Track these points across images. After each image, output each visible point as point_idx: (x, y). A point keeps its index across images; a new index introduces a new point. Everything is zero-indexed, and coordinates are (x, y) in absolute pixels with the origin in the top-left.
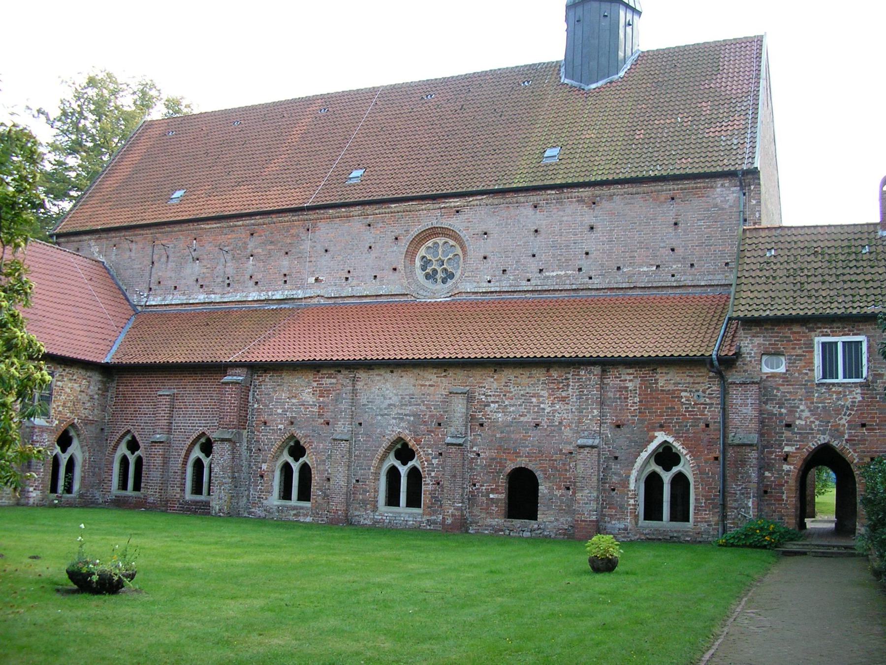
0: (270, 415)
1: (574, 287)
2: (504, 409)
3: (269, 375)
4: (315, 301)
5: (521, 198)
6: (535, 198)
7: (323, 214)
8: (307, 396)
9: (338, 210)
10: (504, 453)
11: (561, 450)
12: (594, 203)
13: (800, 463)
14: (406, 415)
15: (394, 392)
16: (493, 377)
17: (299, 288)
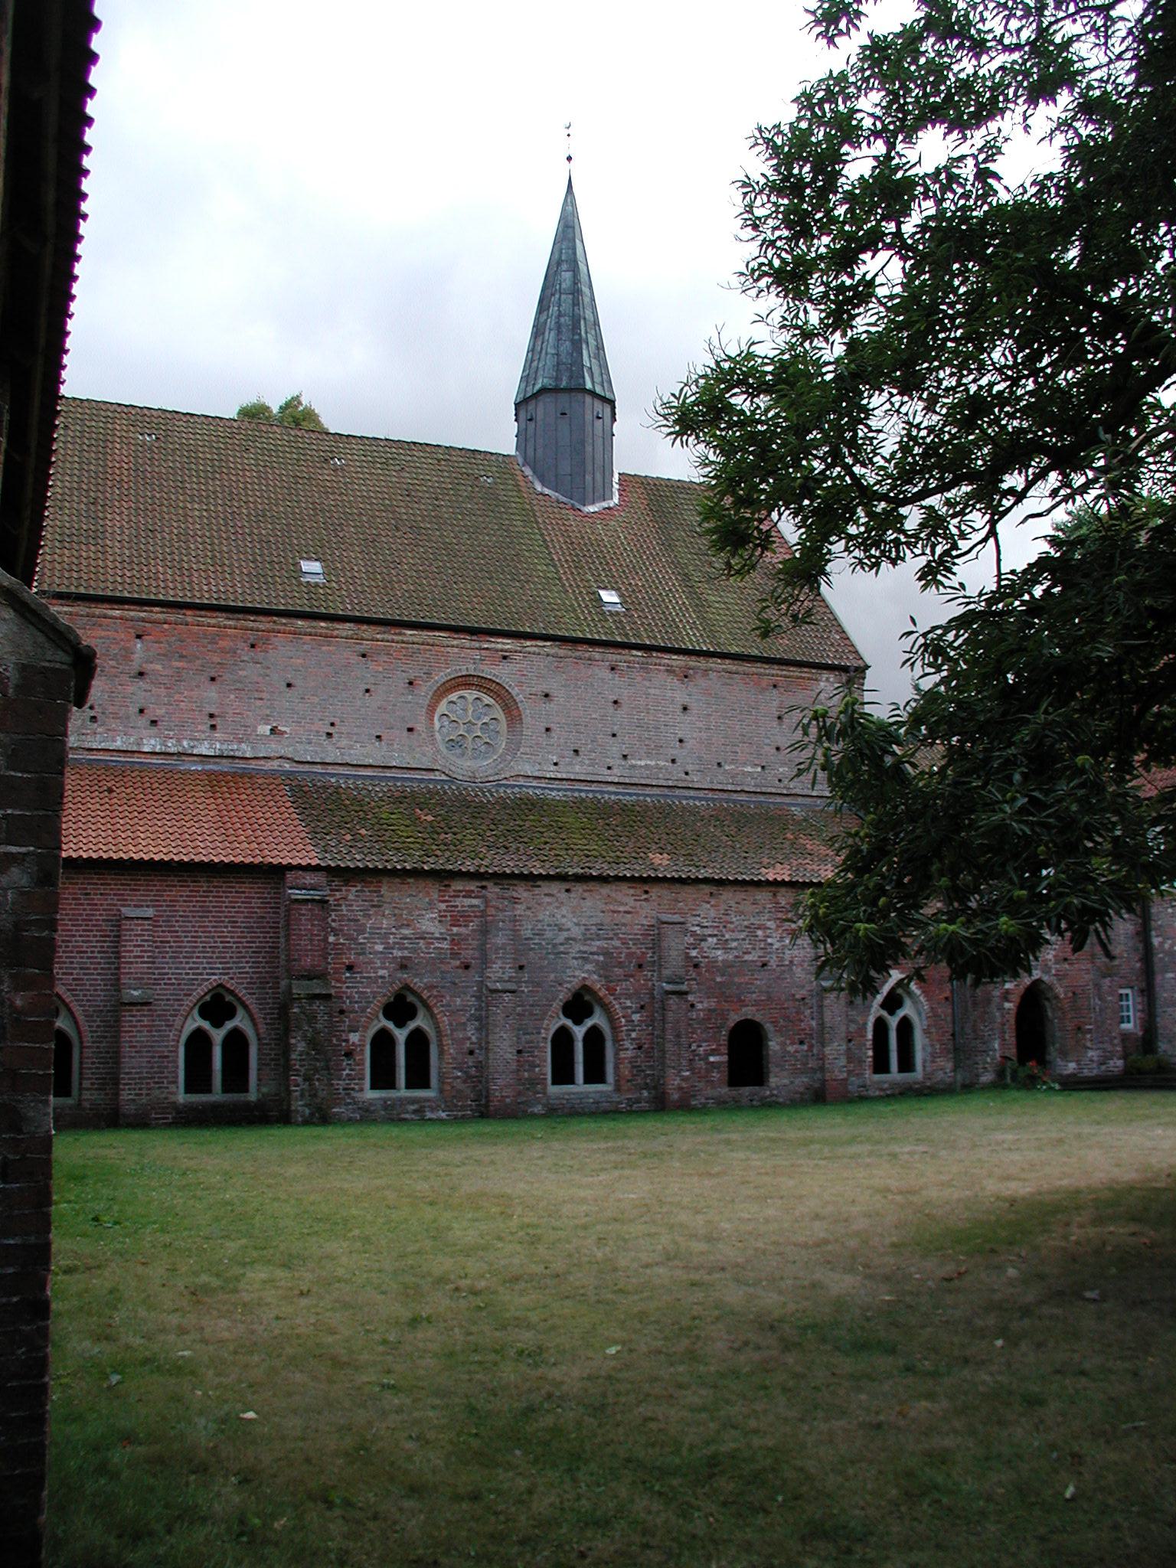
0: (359, 954)
1: (670, 783)
2: (724, 945)
3: (354, 889)
4: (274, 765)
5: (596, 653)
6: (615, 657)
7: (285, 624)
8: (429, 924)
9: (314, 624)
10: (726, 1001)
11: (794, 995)
12: (686, 677)
13: (1018, 1000)
14: (592, 953)
15: (575, 920)
16: (708, 903)
17: (241, 741)
